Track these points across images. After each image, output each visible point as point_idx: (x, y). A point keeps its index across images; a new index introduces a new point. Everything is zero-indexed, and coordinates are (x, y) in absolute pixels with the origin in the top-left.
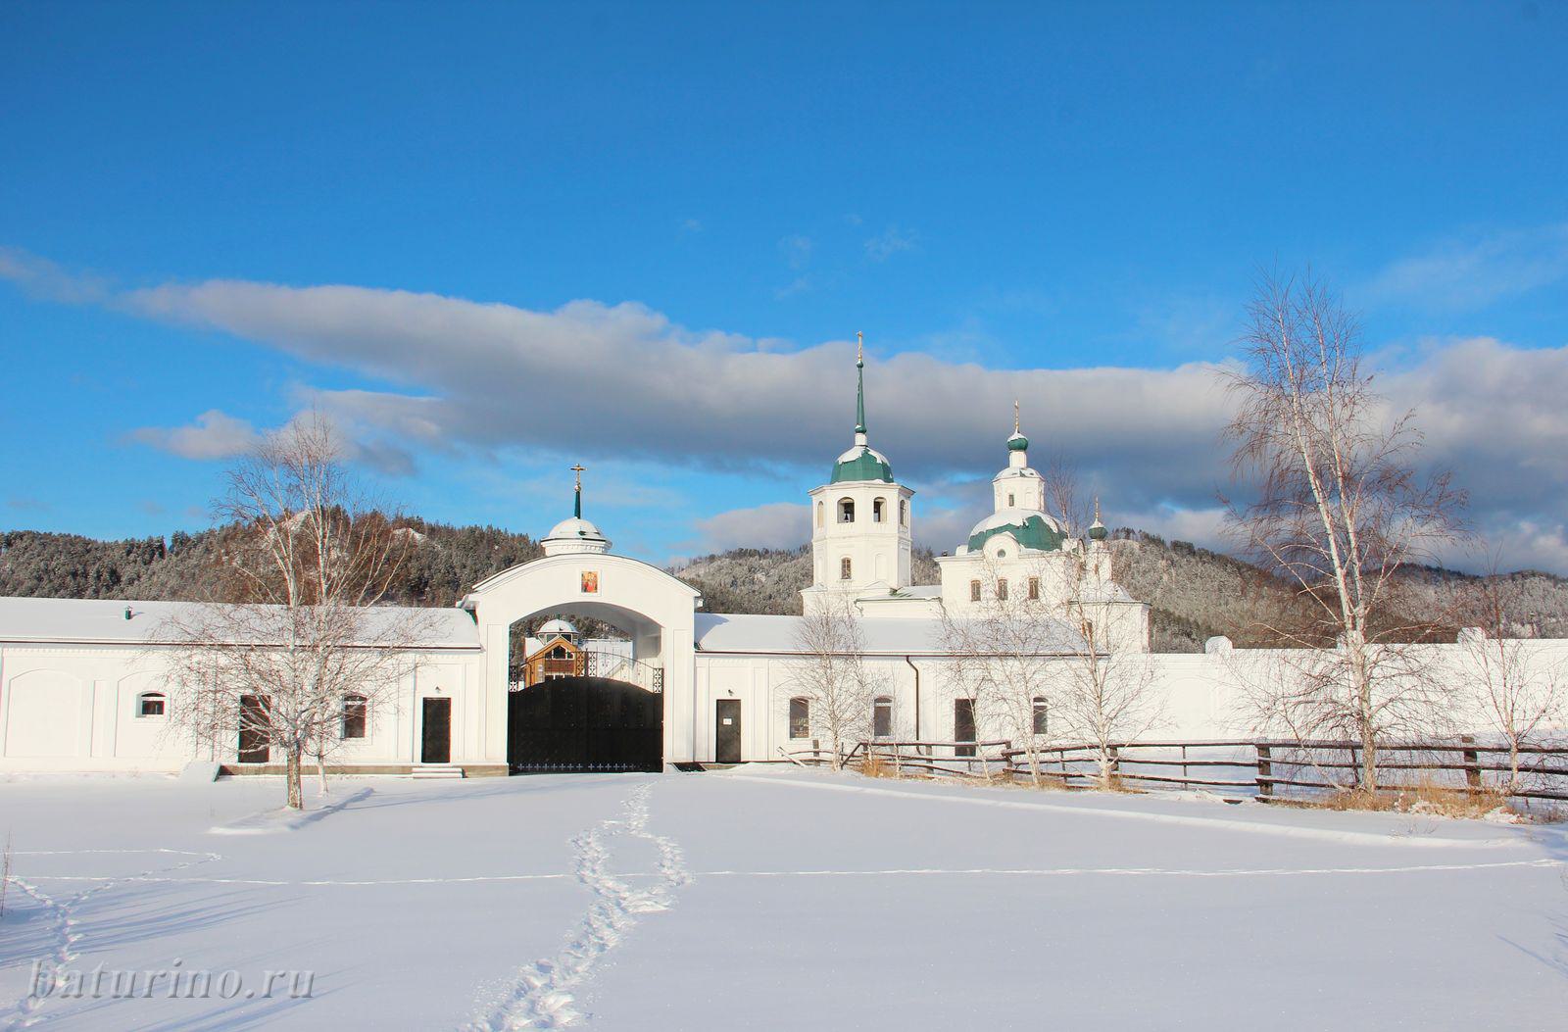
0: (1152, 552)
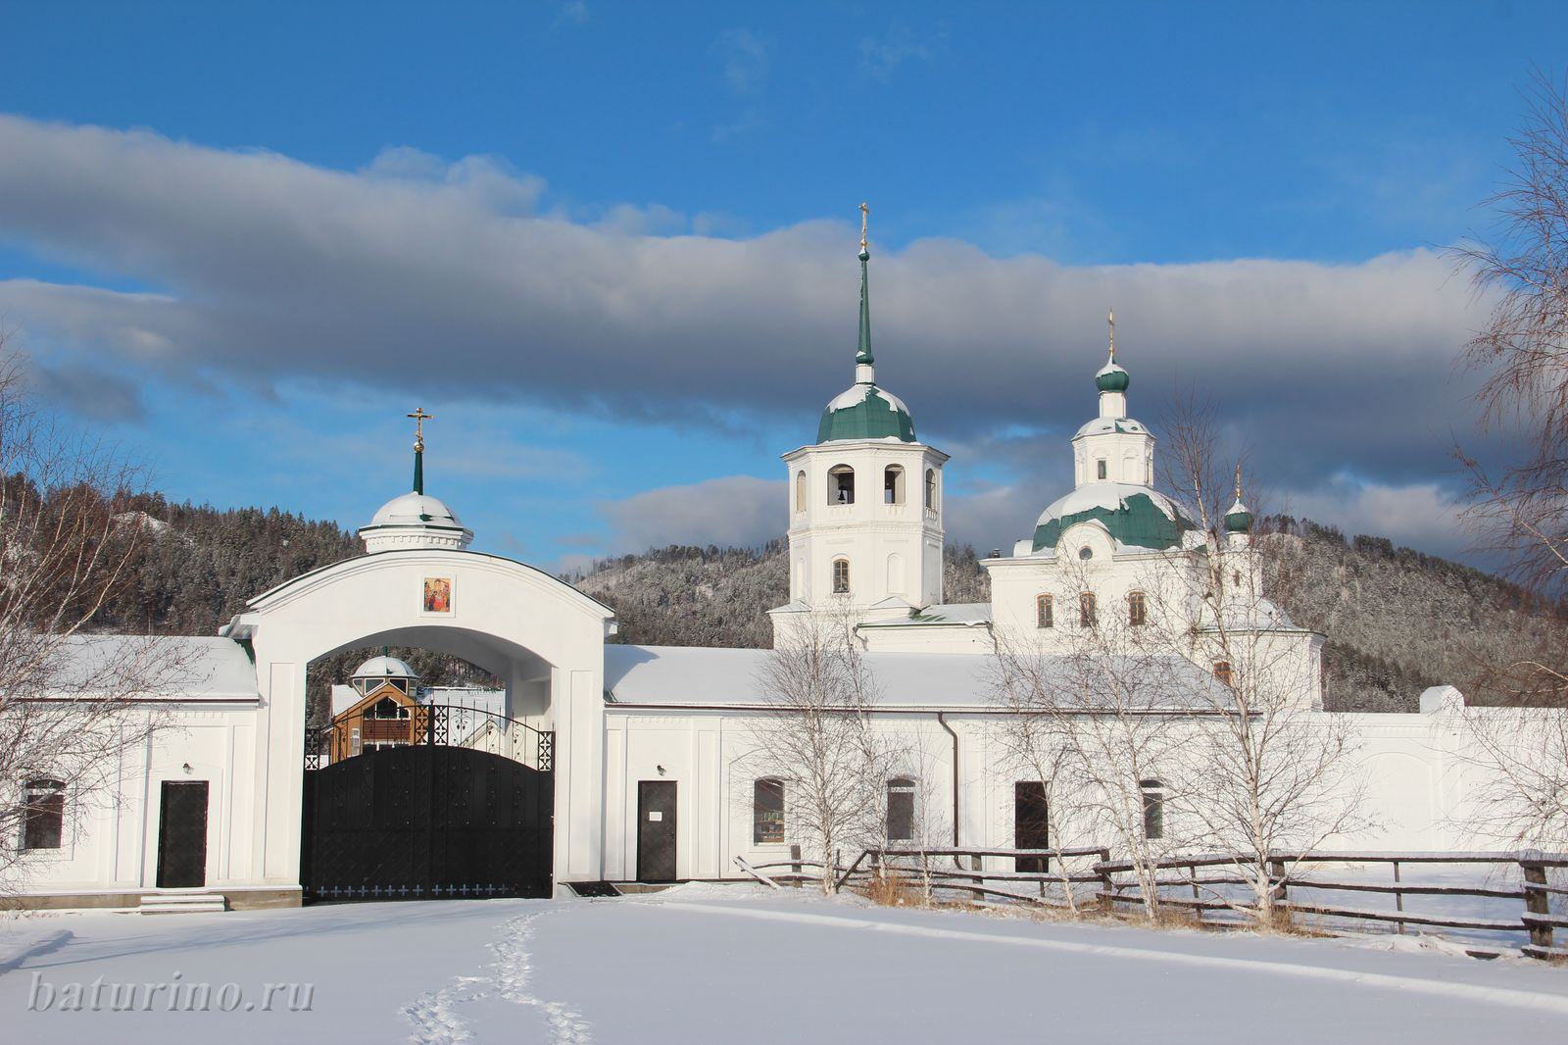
0: (1323, 554)
